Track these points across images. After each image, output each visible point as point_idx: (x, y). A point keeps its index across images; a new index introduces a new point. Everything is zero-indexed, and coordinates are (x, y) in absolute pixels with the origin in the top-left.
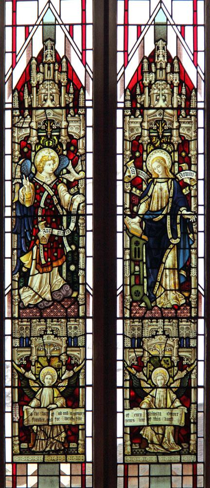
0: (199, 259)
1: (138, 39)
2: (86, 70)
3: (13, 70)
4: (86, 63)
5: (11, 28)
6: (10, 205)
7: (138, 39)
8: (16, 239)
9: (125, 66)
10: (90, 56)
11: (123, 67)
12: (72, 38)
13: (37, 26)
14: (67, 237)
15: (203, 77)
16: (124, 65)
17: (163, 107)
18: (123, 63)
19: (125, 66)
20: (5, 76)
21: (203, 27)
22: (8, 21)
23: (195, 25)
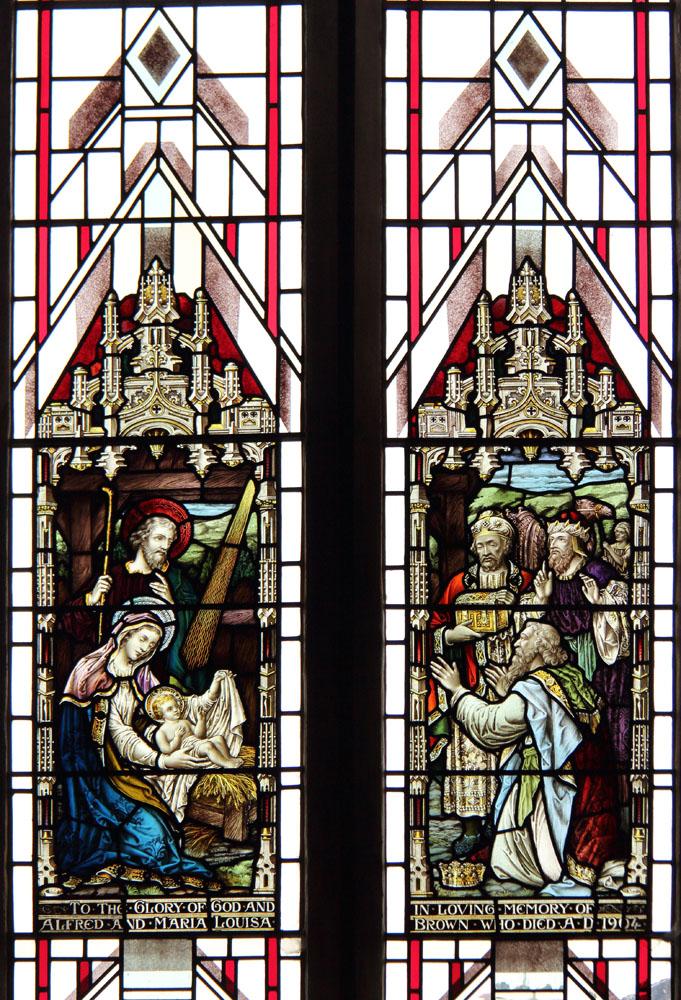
0: (402, 859)
1: (453, 263)
2: (651, 357)
3: (39, 347)
4: (281, 333)
5: (32, 231)
6: (402, 860)
7: (453, 263)
8: (133, 880)
9: (39, 339)
10: (292, 312)
11: (34, 344)
12: (235, 260)
13: (118, 217)
14: (414, 914)
15: (669, 371)
16: (35, 337)
17: (571, 472)
18: (32, 330)
19: (39, 339)
20: (15, 364)
21: (668, 231)
22: (24, 205)
23: (643, 224)
